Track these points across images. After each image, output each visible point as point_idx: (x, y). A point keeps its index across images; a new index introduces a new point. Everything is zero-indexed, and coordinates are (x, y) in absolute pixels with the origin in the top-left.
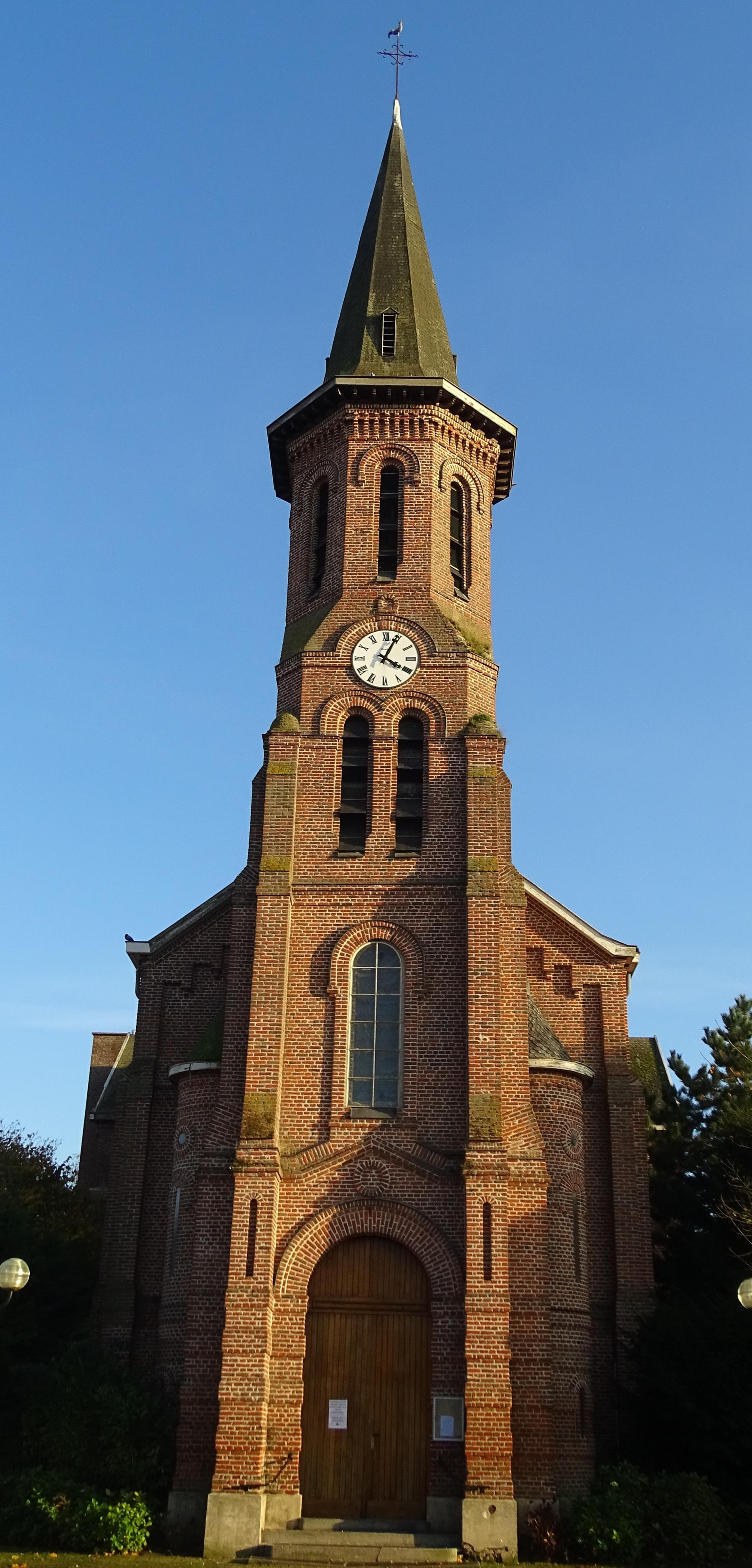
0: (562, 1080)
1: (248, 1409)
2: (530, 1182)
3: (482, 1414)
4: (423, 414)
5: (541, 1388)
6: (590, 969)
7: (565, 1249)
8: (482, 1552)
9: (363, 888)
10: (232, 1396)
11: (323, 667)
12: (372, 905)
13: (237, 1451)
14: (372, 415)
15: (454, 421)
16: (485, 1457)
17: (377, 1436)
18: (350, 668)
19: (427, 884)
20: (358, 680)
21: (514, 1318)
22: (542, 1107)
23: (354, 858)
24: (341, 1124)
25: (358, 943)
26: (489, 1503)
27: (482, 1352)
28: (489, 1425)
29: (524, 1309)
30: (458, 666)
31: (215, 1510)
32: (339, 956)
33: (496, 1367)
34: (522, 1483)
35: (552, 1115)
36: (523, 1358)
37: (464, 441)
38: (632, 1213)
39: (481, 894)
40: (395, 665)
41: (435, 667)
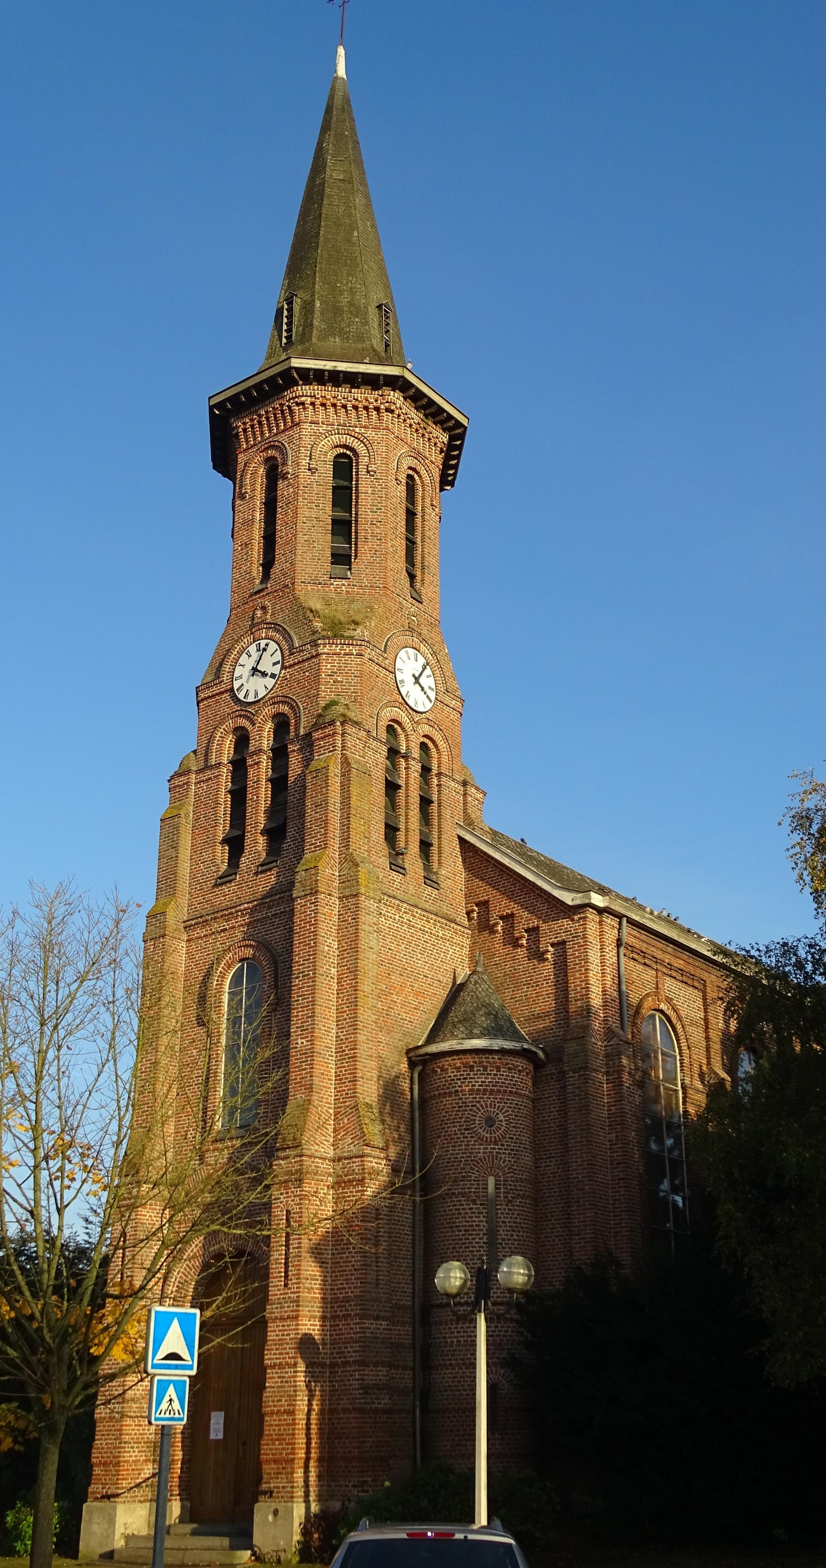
0: (470, 1059)
1: (114, 1426)
2: (350, 1181)
3: (274, 1420)
4: (290, 399)
5: (354, 1389)
6: (554, 925)
7: (474, 1239)
8: (268, 1553)
9: (233, 910)
10: (103, 1415)
11: (213, 696)
12: (242, 925)
13: (105, 1464)
14: (252, 420)
15: (328, 392)
16: (276, 1461)
17: (244, 1444)
18: (232, 690)
19: (280, 893)
20: (237, 701)
21: (335, 1321)
22: (451, 1093)
23: (230, 882)
24: (211, 1147)
25: (229, 966)
26: (274, 1506)
27: (277, 1359)
28: (279, 1430)
29: (341, 1311)
30: (313, 657)
31: (87, 1518)
32: (215, 983)
33: (287, 1373)
34: (336, 1486)
35: (461, 1099)
36: (340, 1360)
37: (344, 406)
38: (587, 1187)
39: (303, 893)
40: (264, 674)
41: (295, 664)
